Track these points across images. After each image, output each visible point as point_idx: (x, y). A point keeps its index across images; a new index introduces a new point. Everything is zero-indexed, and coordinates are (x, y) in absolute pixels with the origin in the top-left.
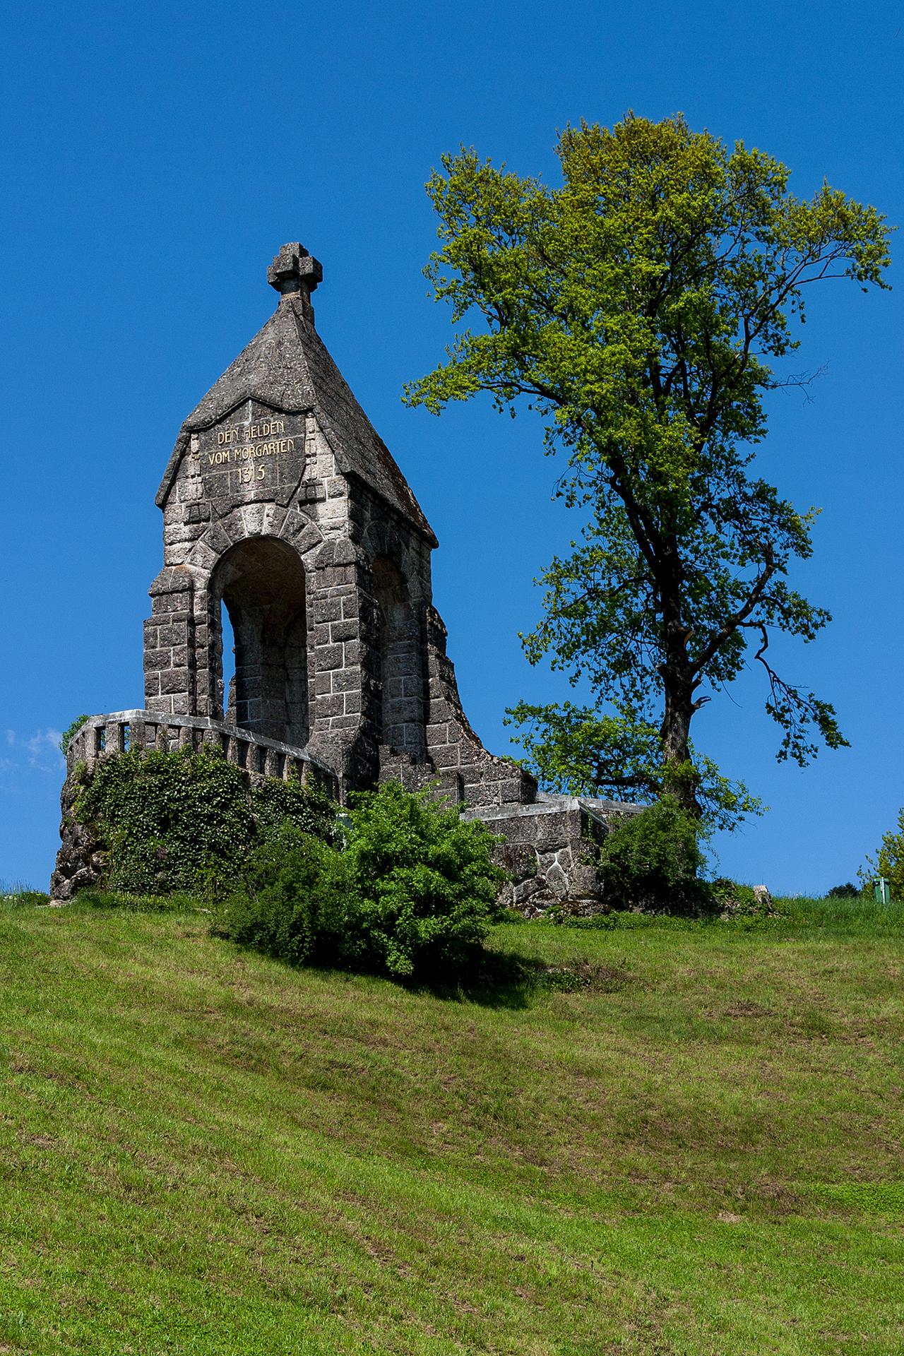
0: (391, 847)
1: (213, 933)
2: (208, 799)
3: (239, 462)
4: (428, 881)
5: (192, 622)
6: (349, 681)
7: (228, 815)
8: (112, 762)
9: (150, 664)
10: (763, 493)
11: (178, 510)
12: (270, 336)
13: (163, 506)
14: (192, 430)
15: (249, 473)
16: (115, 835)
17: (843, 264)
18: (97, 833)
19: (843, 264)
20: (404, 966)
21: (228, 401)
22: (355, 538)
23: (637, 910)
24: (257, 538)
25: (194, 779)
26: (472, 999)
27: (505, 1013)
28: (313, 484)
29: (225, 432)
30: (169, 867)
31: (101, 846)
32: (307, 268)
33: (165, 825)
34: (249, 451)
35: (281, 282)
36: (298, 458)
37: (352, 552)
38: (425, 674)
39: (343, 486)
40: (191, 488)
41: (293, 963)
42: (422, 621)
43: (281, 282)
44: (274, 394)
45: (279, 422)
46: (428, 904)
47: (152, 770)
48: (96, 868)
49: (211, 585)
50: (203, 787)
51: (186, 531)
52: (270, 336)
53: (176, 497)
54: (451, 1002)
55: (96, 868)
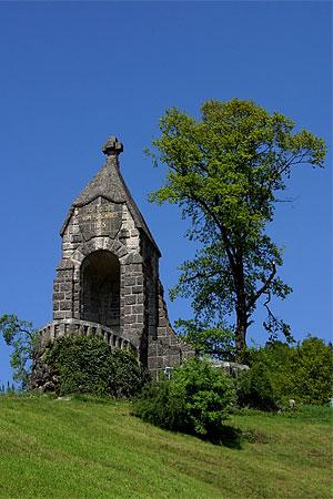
0: (198, 383)
1: (132, 415)
2: (98, 356)
3: (95, 220)
4: (213, 397)
5: (74, 282)
6: (139, 310)
7: (105, 363)
8: (62, 339)
9: (55, 298)
10: (266, 240)
11: (69, 237)
12: (105, 172)
13: (62, 235)
14: (75, 206)
15: (99, 225)
16: (63, 369)
17: (307, 158)
18: (55, 368)
19: (307, 158)
20: (203, 431)
21: (91, 196)
22: (141, 253)
23: (246, 408)
24: (101, 250)
25: (94, 348)
26: (225, 445)
27: (236, 451)
28: (124, 231)
29: (88, 208)
30: (83, 383)
31: (58, 373)
32: (119, 147)
33: (83, 366)
34: (99, 216)
35: (107, 151)
36: (119, 220)
37: (141, 259)
38: (157, 307)
39: (137, 233)
40: (75, 229)
41: (162, 427)
42: (157, 286)
43: (107, 151)
44: (110, 195)
45: (112, 206)
46: (213, 406)
47: (77, 343)
48: (54, 382)
49: (81, 268)
50: (97, 351)
51: (72, 246)
52: (105, 172)
53: (68, 232)
54: (223, 448)
55: (54, 382)
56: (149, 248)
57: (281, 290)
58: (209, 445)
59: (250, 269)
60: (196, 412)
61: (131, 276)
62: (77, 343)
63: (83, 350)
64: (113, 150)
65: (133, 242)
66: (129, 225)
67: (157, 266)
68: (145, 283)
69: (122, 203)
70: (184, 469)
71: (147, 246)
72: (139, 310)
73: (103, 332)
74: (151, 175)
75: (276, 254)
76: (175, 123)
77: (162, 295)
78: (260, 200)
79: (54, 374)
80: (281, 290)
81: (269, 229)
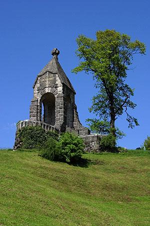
0: (67, 141)
1: (39, 155)
5: (37, 106)
9: (31, 112)
10: (126, 86)
12: (51, 62)
20: (69, 161)
24: (48, 93)
28: (57, 84)
31: (22, 141)
33: (32, 138)
35: (53, 54)
36: (55, 80)
39: (62, 85)
40: (38, 85)
43: (53, 54)
45: (52, 75)
46: (73, 150)
47: (30, 129)
49: (40, 100)
50: (38, 132)
52: (51, 62)
56: (69, 92)
57: (132, 105)
58: (72, 167)
59: (119, 96)
60: (66, 154)
61: (59, 102)
62: (30, 129)
63: (32, 132)
64: (56, 54)
65: (60, 89)
66: (59, 82)
67: (74, 98)
68: (64, 104)
69: (56, 74)
70: (44, 176)
71: (67, 90)
72: (62, 115)
73: (42, 124)
74: (72, 61)
75: (131, 91)
76: (82, 41)
77: (76, 110)
78: (121, 71)
79: (20, 142)
80: (132, 105)
81: (126, 81)
